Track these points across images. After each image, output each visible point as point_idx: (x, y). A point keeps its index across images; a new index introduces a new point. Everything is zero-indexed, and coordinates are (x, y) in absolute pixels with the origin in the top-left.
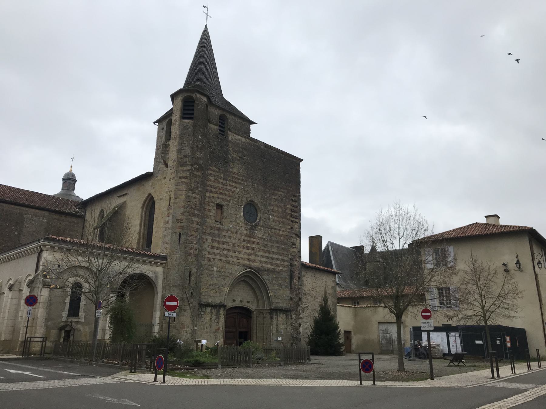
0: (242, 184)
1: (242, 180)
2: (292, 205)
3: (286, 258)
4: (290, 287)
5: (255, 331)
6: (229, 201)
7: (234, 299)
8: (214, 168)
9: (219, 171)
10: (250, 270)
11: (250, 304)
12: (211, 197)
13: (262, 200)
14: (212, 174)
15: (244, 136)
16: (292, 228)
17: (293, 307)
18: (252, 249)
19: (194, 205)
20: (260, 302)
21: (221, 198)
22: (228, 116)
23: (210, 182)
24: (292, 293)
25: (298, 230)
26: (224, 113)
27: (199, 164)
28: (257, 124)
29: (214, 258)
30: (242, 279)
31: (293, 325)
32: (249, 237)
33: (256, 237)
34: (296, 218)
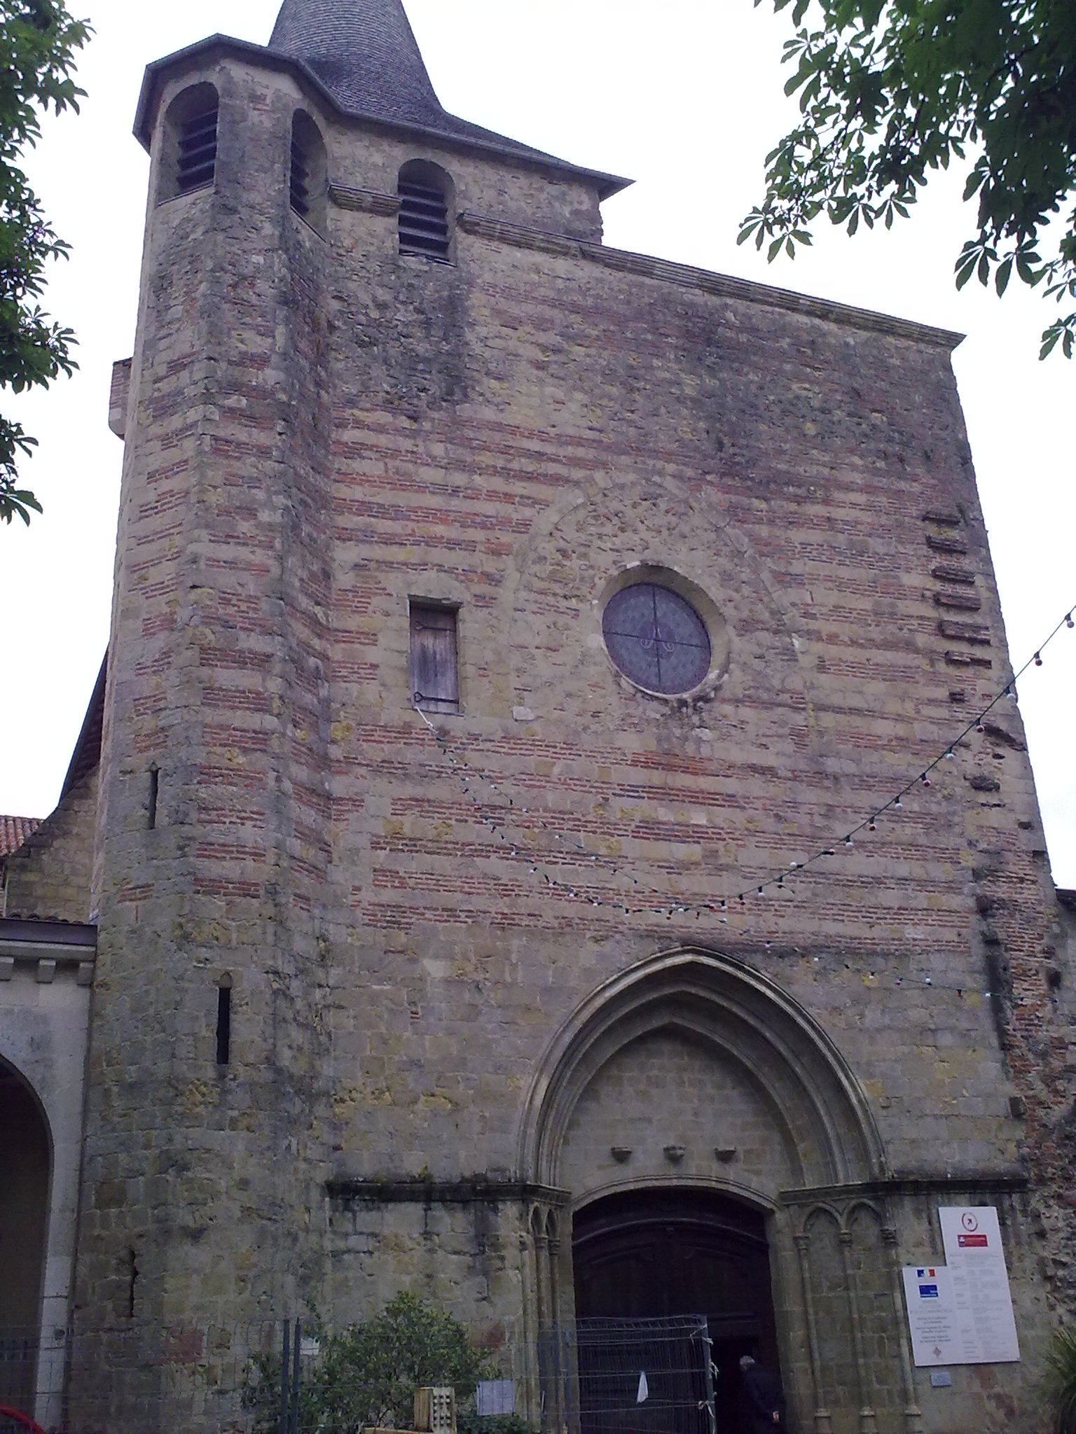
0: (577, 483)
1: (575, 462)
2: (934, 571)
3: (940, 871)
4: (995, 1042)
5: (796, 1335)
6: (493, 580)
7: (621, 1145)
8: (383, 417)
9: (415, 426)
10: (688, 958)
11: (740, 1165)
12: (373, 565)
13: (721, 560)
14: (371, 448)
15: (562, 246)
16: (956, 698)
17: (1038, 1162)
18: (694, 835)
19: (227, 602)
20: (801, 1147)
21: (440, 568)
22: (455, 167)
23: (359, 488)
24: (1015, 1070)
25: (1000, 706)
26: (429, 155)
27: (254, 388)
28: (633, 182)
29: (421, 903)
30: (655, 1023)
31: (1061, 1273)
32: (657, 765)
33: (713, 766)
34: (973, 641)
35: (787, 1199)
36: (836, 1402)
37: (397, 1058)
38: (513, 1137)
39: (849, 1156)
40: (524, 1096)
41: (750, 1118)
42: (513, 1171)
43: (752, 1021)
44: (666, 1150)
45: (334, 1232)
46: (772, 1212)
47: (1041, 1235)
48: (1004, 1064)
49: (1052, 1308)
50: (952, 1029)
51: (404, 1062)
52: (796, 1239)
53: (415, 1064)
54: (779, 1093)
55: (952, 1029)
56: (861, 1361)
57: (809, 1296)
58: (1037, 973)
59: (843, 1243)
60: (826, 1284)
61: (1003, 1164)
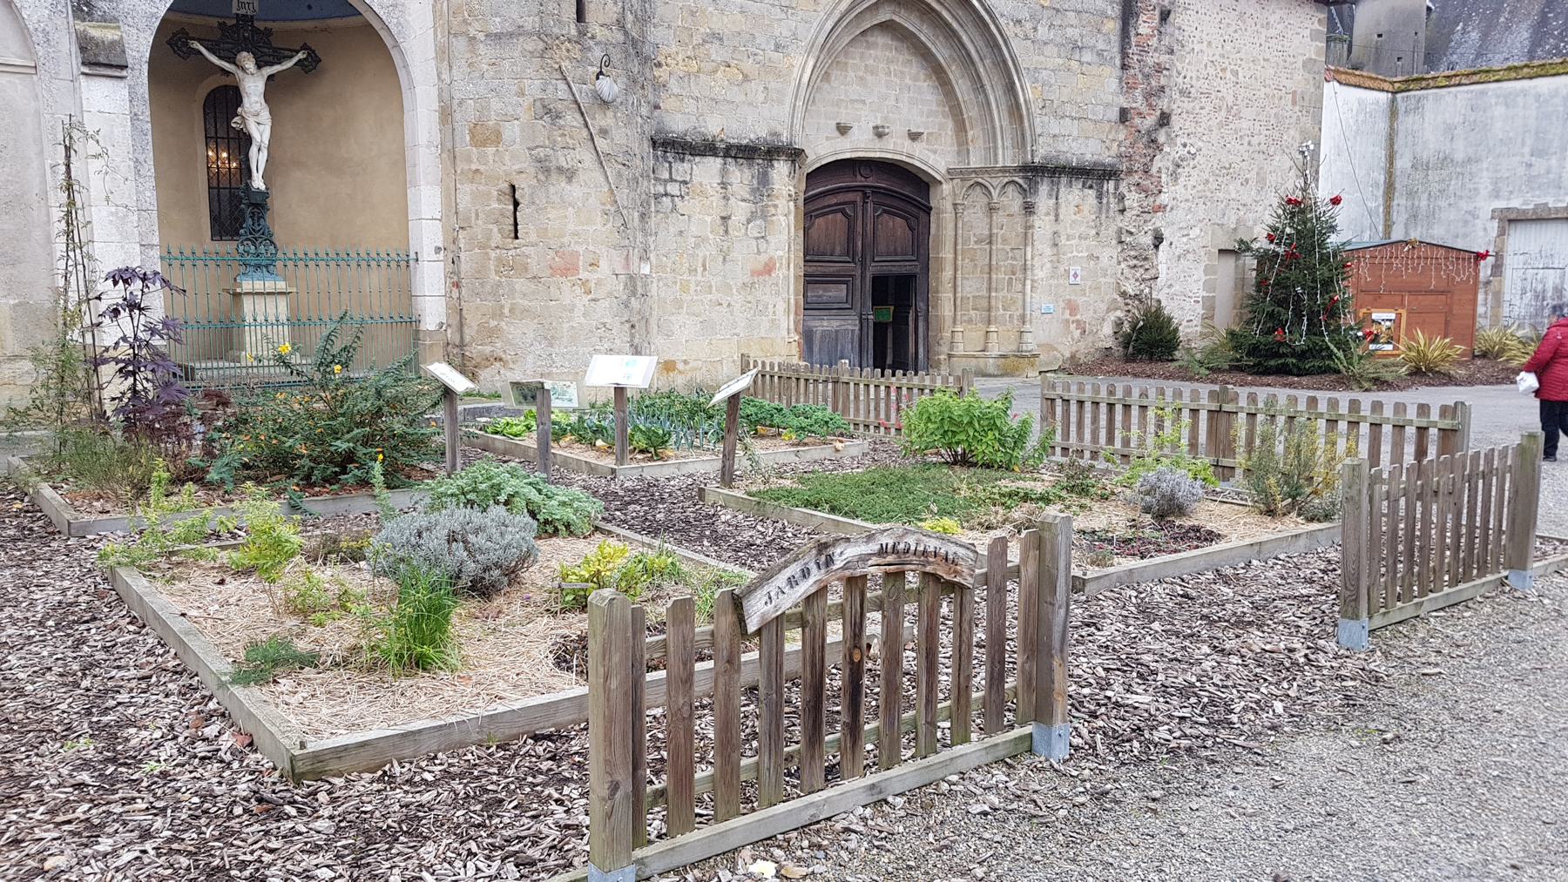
4: (1118, 62)
24: (1128, 87)
35: (951, 173)
36: (970, 321)
37: (702, 30)
38: (787, 108)
39: (1008, 143)
40: (796, 72)
41: (934, 108)
42: (785, 138)
43: (955, 25)
44: (876, 128)
45: (656, 179)
46: (940, 183)
47: (1122, 211)
48: (1121, 80)
49: (1119, 263)
50: (1092, 48)
51: (707, 35)
52: (955, 205)
53: (717, 37)
54: (962, 87)
55: (1092, 48)
56: (993, 294)
57: (959, 247)
58: (1154, 9)
59: (991, 209)
60: (973, 239)
61: (1107, 158)
